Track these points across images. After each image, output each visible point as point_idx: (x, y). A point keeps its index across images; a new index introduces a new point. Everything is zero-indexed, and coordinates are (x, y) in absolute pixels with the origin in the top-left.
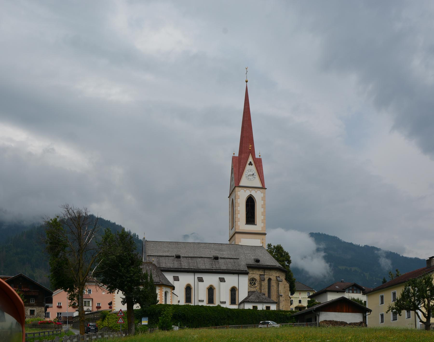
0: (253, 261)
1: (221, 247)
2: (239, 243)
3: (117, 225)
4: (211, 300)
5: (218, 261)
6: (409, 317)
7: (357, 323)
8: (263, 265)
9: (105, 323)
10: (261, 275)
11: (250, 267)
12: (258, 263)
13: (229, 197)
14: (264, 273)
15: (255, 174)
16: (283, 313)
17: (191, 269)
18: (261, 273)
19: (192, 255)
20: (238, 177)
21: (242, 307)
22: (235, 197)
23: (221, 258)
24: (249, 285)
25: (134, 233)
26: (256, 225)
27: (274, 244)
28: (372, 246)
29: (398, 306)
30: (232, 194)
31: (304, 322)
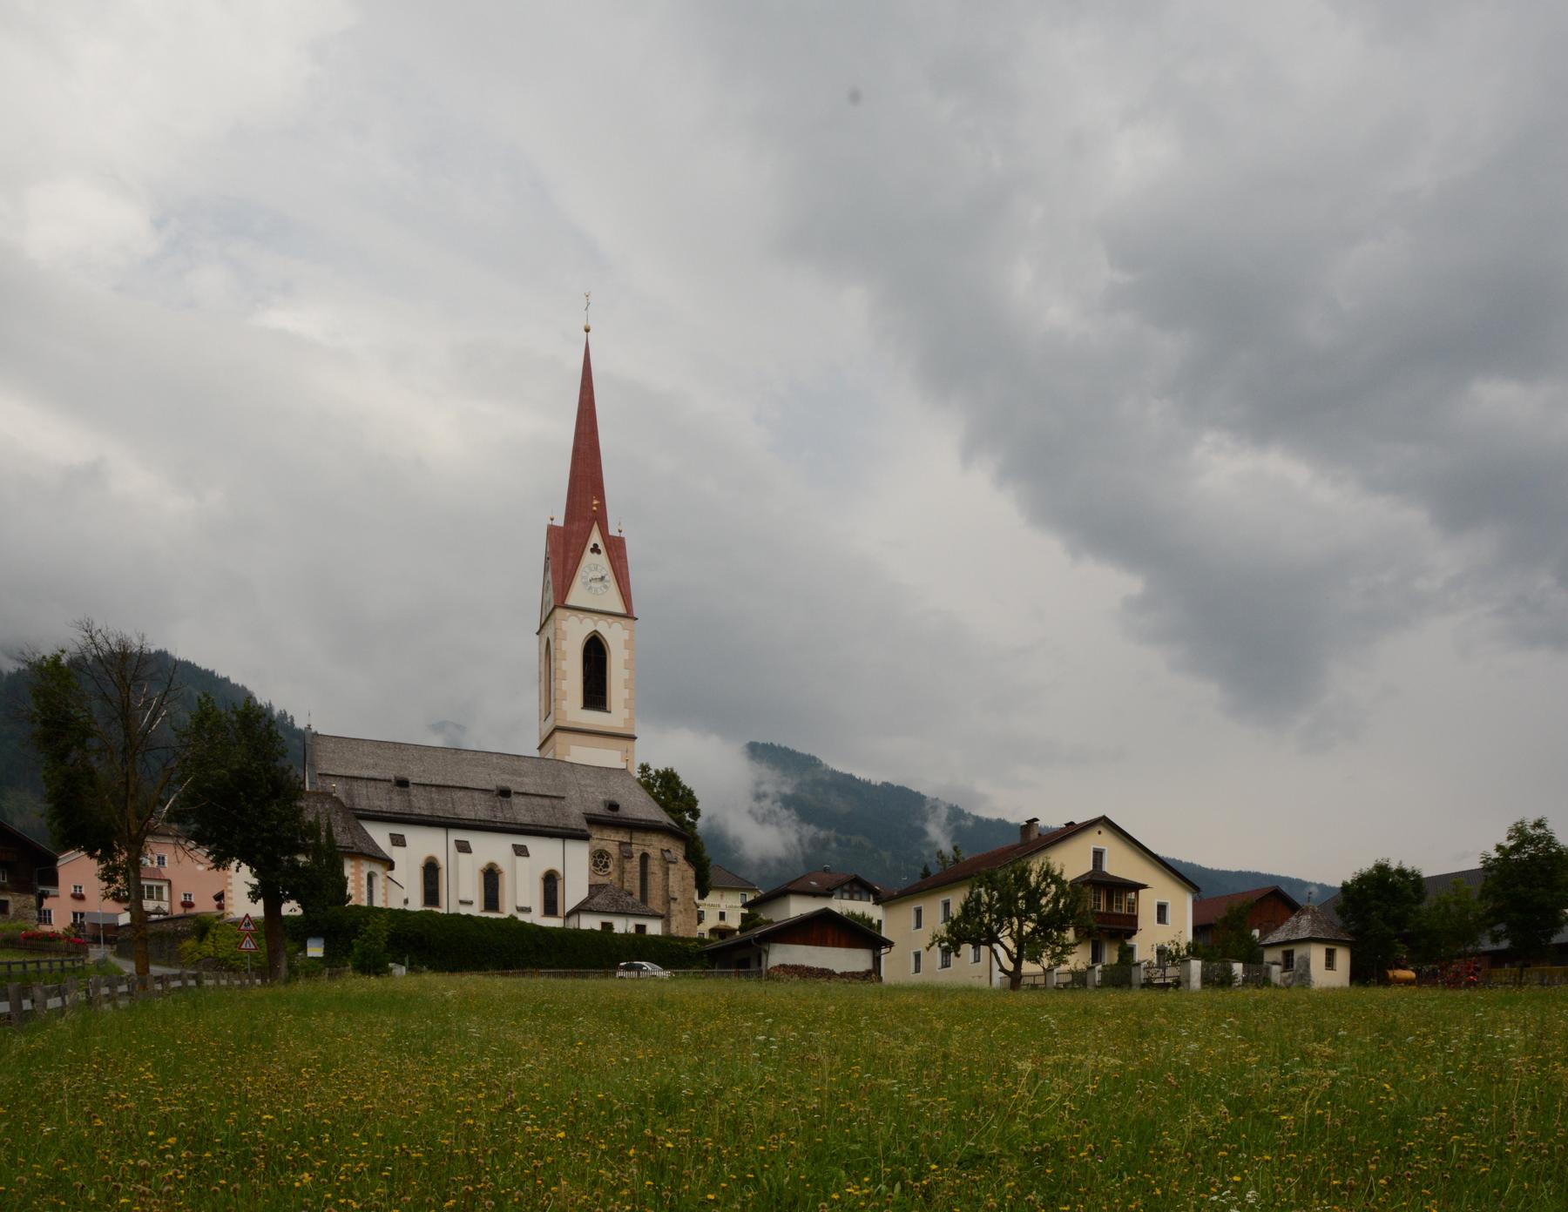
0: (602, 807)
1: (516, 763)
3: (234, 684)
7: (858, 973)
8: (628, 819)
10: (621, 844)
11: (594, 821)
12: (615, 814)
13: (537, 634)
14: (631, 839)
15: (607, 578)
16: (679, 943)
17: (438, 817)
18: (623, 837)
19: (439, 780)
21: (572, 923)
22: (555, 634)
24: (593, 868)
26: (610, 712)
27: (658, 765)
28: (901, 784)
29: (954, 935)
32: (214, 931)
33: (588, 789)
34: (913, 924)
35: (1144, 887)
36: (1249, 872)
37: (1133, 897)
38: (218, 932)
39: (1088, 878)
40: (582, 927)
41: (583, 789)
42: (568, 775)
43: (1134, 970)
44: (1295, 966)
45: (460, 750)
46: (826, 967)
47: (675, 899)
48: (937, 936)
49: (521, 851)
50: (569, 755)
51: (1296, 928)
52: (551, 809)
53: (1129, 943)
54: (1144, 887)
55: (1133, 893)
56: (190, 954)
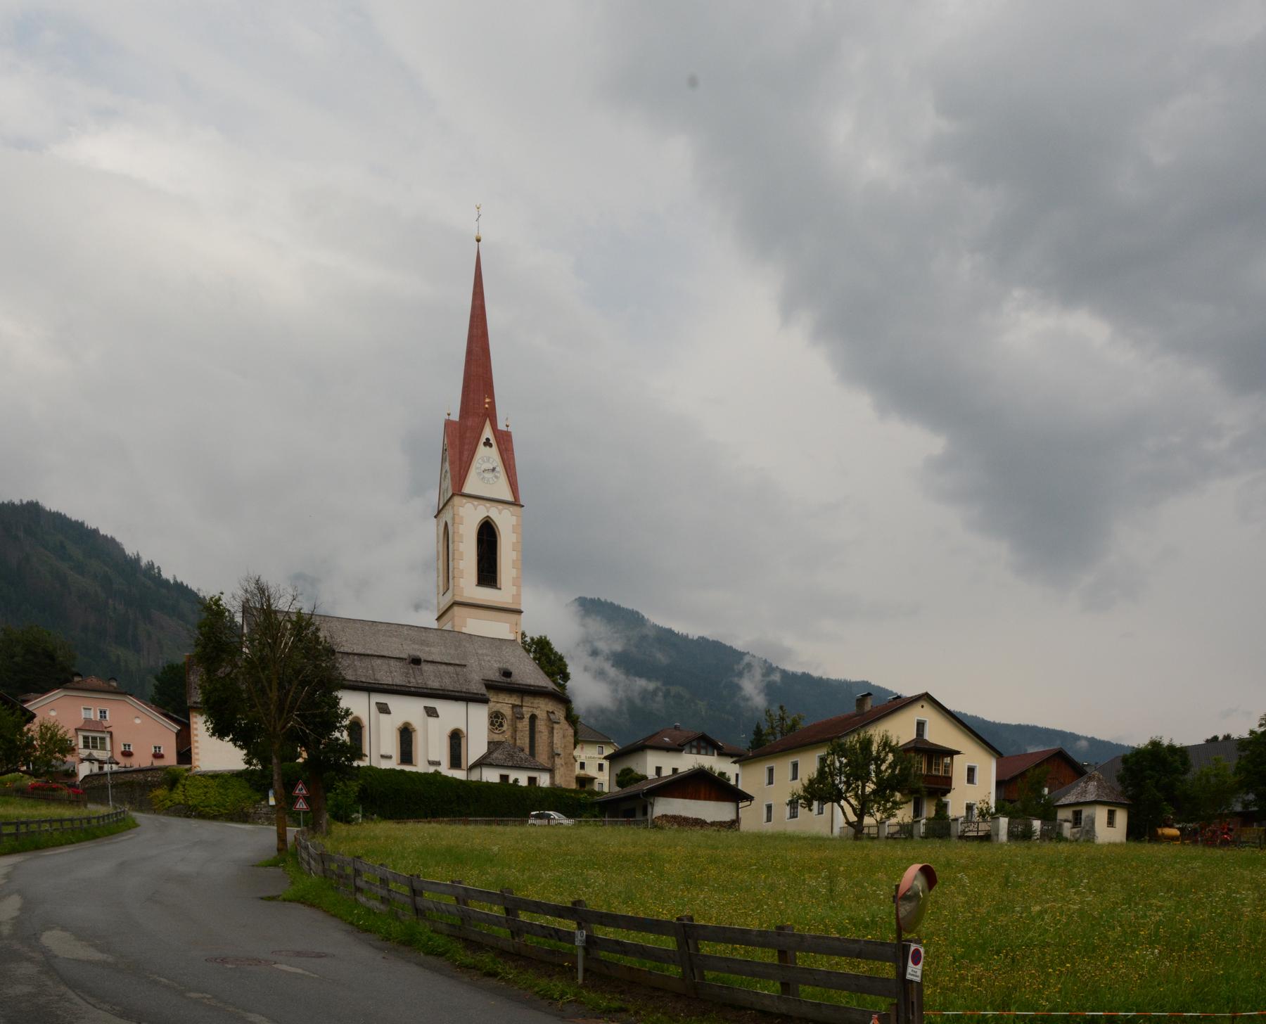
0: (497, 674)
1: (424, 634)
2: (463, 628)
3: (103, 535)
4: (407, 755)
5: (421, 669)
6: (821, 812)
7: (724, 822)
8: (519, 684)
9: (176, 795)
10: (514, 706)
11: (491, 686)
12: (509, 680)
13: (435, 517)
14: (522, 702)
15: (497, 469)
16: (573, 795)
17: (362, 682)
18: (515, 700)
19: (361, 650)
20: (460, 473)
21: (475, 776)
22: (453, 519)
23: (428, 662)
24: (490, 727)
25: (148, 562)
26: (500, 589)
27: (534, 633)
28: (715, 639)
29: (809, 793)
30: (443, 511)
31: (617, 817)
32: (183, 782)
33: (485, 658)
34: (766, 781)
35: (958, 753)
36: (1028, 726)
37: (949, 762)
38: (187, 782)
39: (912, 745)
40: (484, 780)
41: (481, 658)
42: (468, 645)
43: (953, 826)
44: (1083, 823)
45: (375, 622)
46: (699, 817)
47: (559, 755)
48: (795, 794)
49: (431, 712)
50: (465, 627)
51: (1085, 792)
52: (455, 676)
53: (944, 799)
54: (958, 753)
55: (949, 758)
56: (162, 801)
